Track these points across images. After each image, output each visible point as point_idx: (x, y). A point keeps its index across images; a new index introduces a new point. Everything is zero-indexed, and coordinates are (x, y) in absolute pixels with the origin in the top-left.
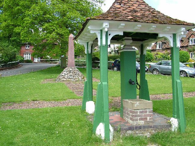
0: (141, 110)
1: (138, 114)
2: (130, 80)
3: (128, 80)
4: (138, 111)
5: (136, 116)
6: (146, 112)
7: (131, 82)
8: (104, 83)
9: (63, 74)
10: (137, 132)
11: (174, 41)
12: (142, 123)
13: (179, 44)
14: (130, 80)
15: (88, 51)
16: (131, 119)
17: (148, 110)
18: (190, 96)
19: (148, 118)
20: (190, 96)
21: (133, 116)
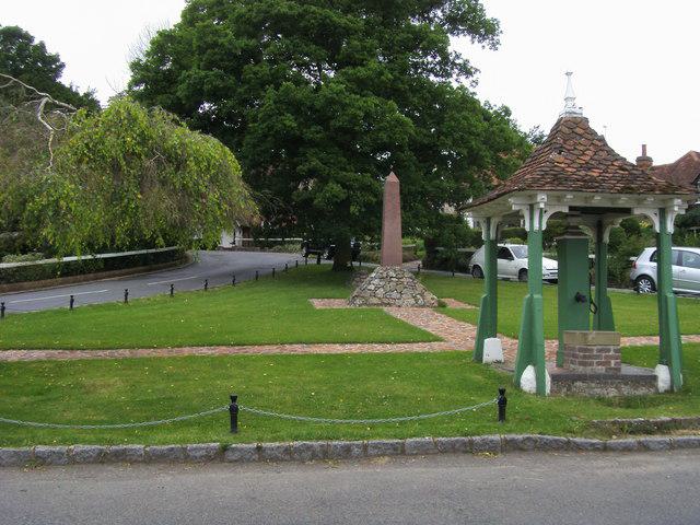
0: (600, 347)
1: (595, 353)
2: (494, 46)
3: (574, 295)
4: (595, 348)
5: (590, 357)
6: (609, 351)
7: (579, 298)
8: (535, 296)
9: (372, 287)
10: (593, 385)
11: (661, 223)
12: (601, 370)
13: (670, 228)
14: (494, 46)
15: (488, 235)
16: (581, 364)
17: (612, 347)
18: (695, 339)
19: (613, 362)
20: (695, 339)
21: (585, 357)
